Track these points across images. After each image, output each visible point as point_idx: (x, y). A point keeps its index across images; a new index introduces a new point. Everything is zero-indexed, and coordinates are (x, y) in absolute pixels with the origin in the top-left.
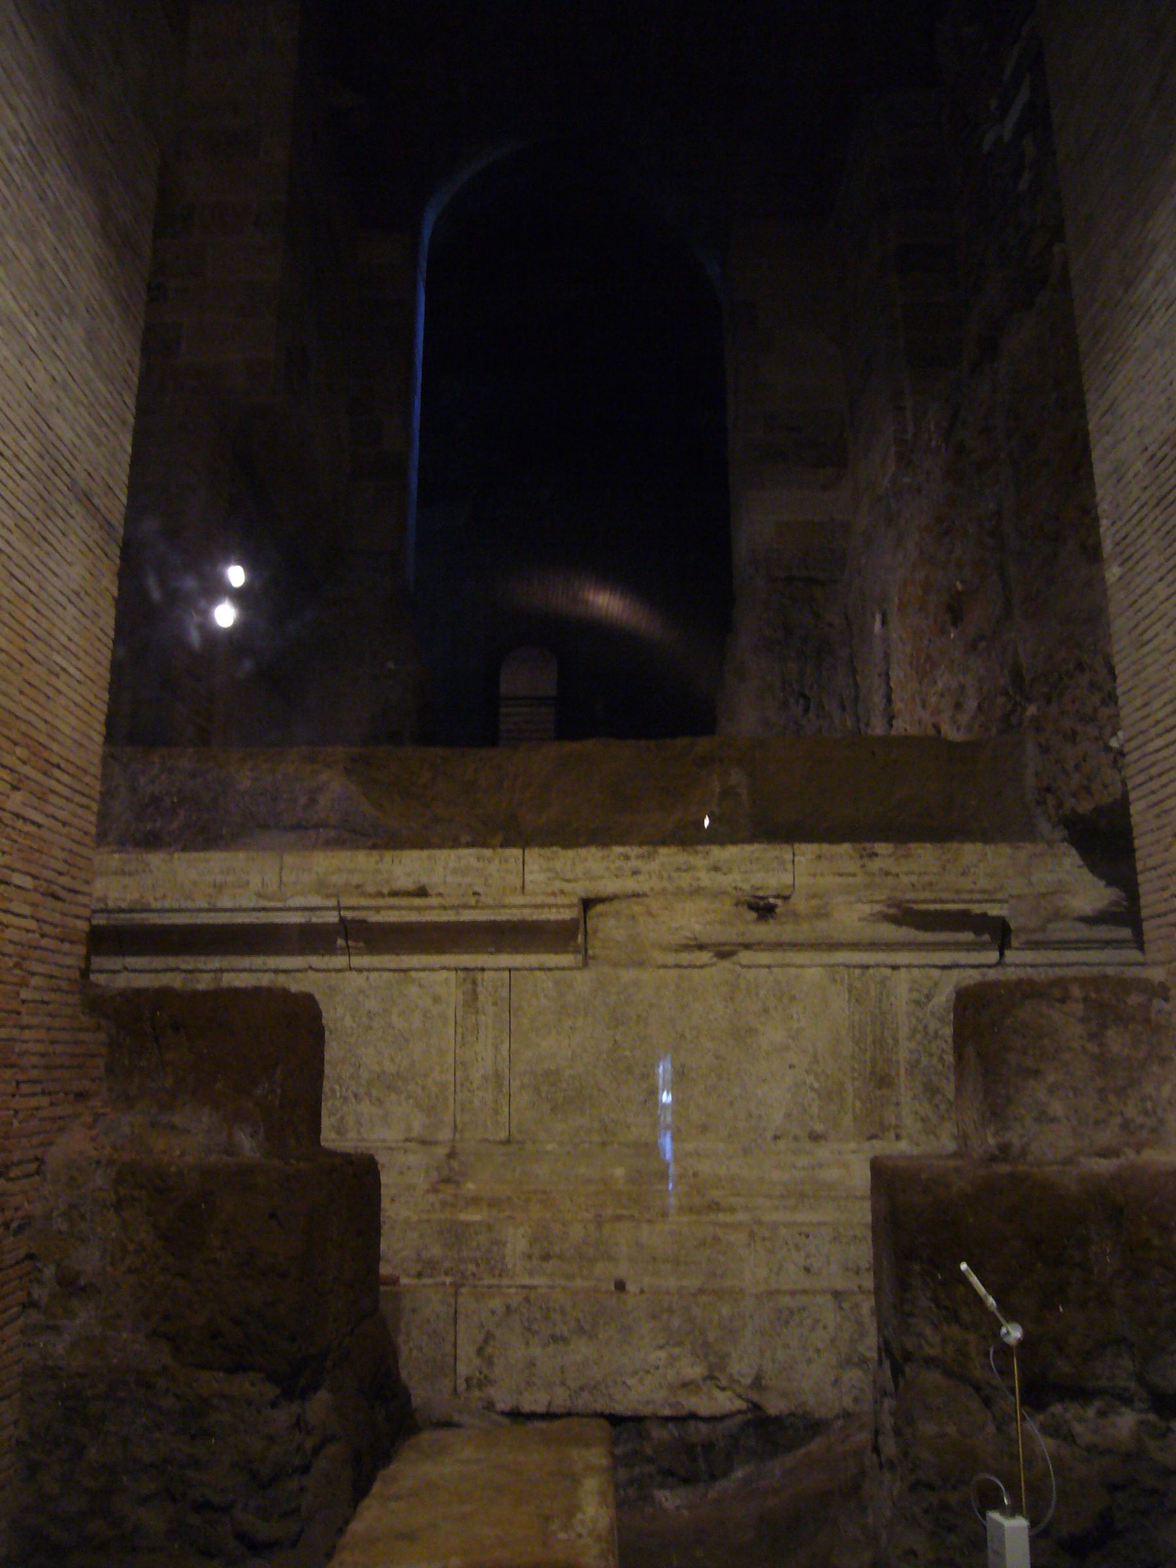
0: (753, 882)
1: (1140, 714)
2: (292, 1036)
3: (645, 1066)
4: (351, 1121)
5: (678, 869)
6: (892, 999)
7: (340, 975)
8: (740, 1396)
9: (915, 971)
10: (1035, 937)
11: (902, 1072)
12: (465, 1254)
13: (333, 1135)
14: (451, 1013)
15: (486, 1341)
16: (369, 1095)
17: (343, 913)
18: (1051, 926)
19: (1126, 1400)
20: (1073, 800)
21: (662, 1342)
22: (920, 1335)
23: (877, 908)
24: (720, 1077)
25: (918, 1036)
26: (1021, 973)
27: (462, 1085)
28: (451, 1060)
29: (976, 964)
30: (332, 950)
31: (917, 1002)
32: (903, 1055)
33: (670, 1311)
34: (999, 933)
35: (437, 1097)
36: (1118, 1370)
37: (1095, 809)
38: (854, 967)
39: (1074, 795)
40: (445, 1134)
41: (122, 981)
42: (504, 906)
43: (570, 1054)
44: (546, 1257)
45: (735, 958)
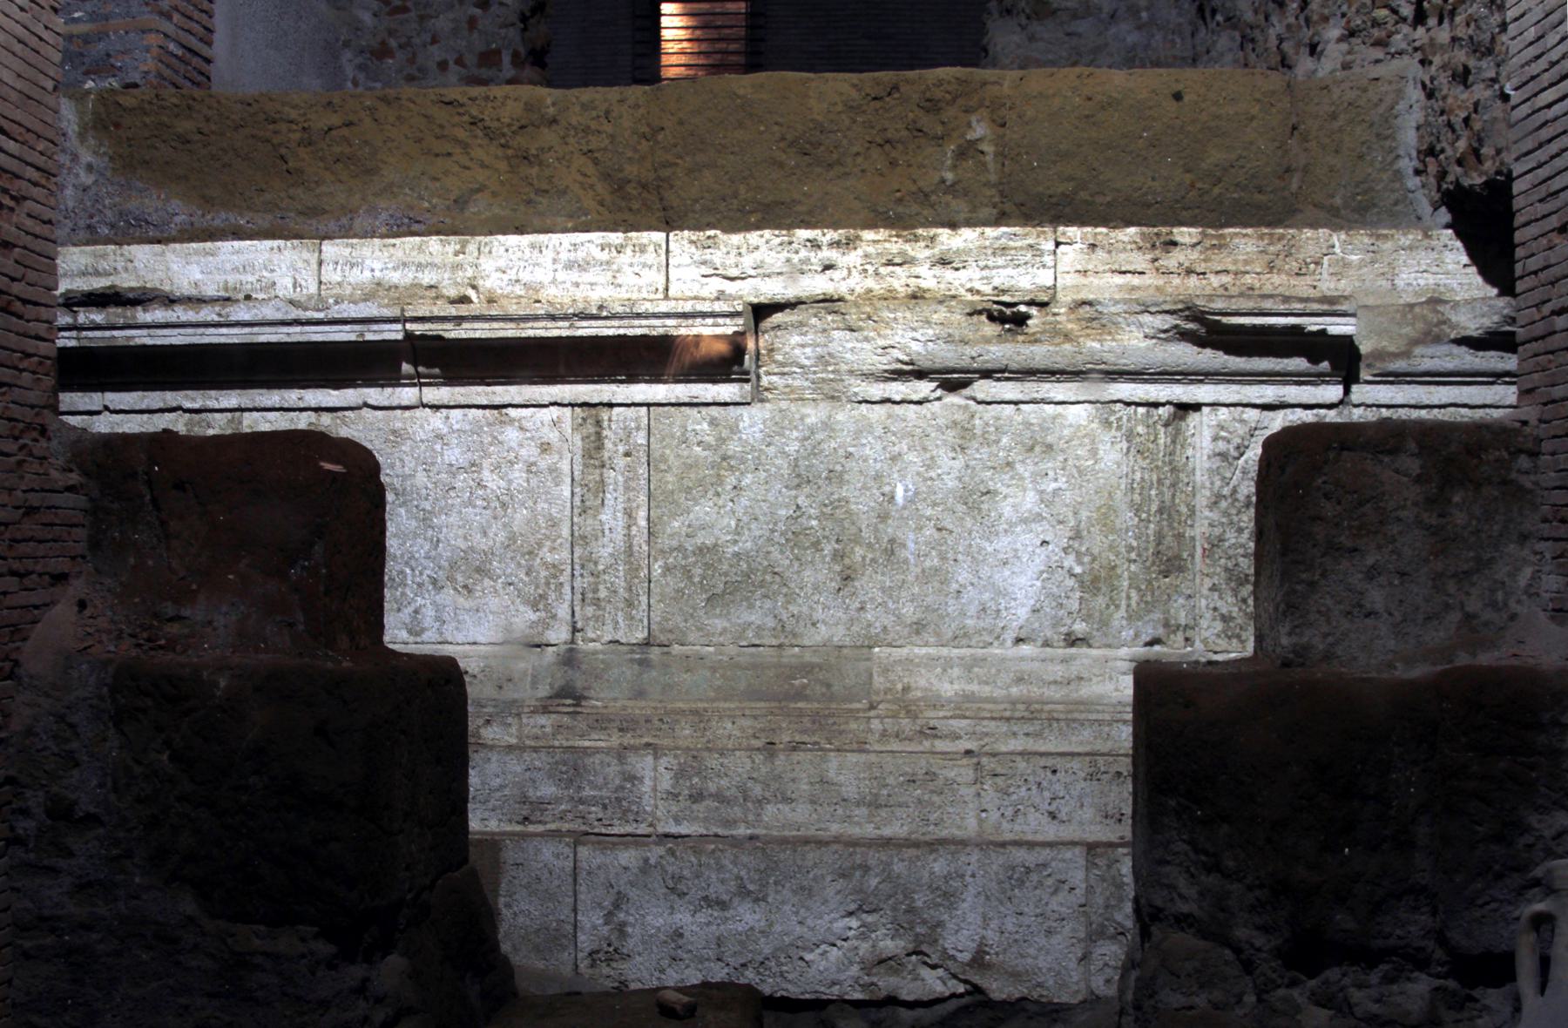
0: (997, 282)
1: (1532, 51)
2: (345, 495)
3: (838, 541)
4: (429, 612)
5: (890, 263)
6: (1190, 452)
7: (407, 414)
8: (955, 976)
9: (1223, 413)
10: (1400, 365)
11: (1199, 551)
12: (588, 792)
13: (404, 635)
14: (565, 466)
15: (617, 906)
16: (450, 579)
17: (408, 326)
18: (1418, 351)
19: (1421, 963)
20: (1459, 170)
21: (853, 907)
22: (1172, 887)
23: (1170, 321)
24: (943, 558)
25: (1224, 504)
26: (1371, 416)
27: (583, 567)
28: (566, 532)
29: (1313, 399)
30: (395, 380)
31: (1223, 456)
32: (1199, 530)
33: (866, 869)
34: (1343, 360)
35: (548, 584)
36: (1412, 926)
37: (1486, 183)
38: (1138, 404)
39: (1460, 162)
40: (558, 634)
41: (103, 425)
42: (638, 316)
43: (733, 523)
44: (697, 797)
45: (967, 392)
